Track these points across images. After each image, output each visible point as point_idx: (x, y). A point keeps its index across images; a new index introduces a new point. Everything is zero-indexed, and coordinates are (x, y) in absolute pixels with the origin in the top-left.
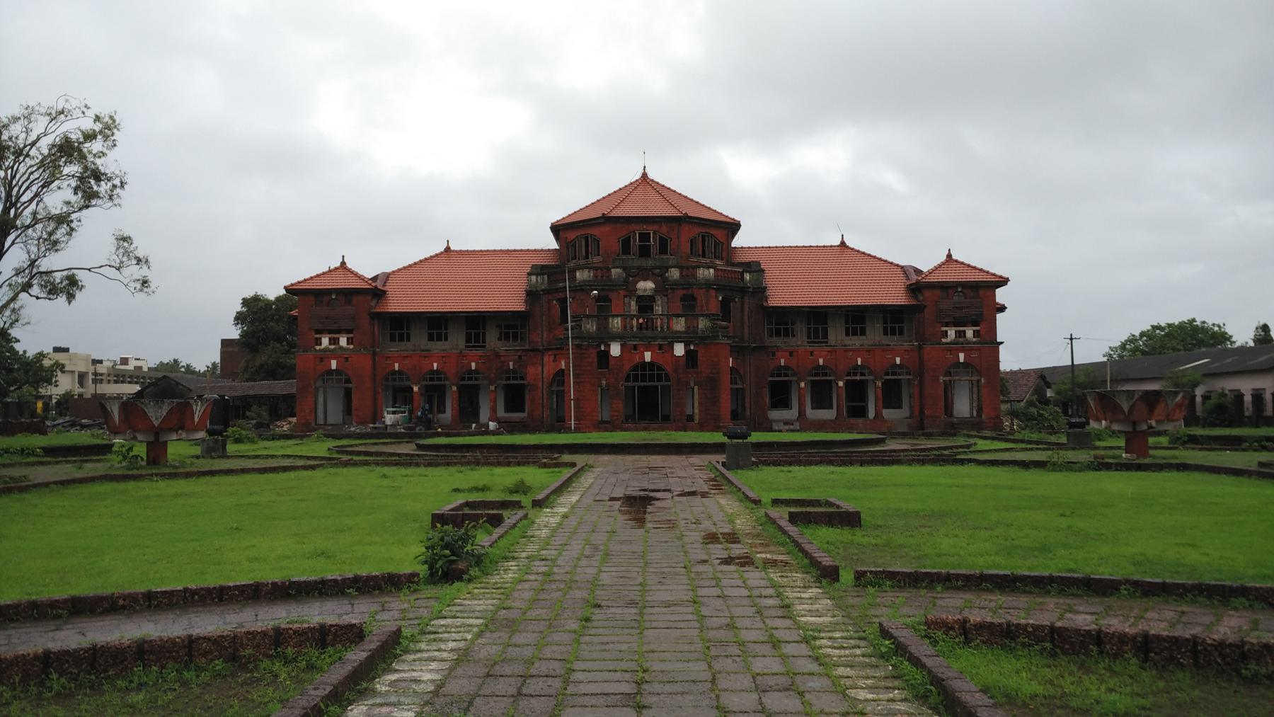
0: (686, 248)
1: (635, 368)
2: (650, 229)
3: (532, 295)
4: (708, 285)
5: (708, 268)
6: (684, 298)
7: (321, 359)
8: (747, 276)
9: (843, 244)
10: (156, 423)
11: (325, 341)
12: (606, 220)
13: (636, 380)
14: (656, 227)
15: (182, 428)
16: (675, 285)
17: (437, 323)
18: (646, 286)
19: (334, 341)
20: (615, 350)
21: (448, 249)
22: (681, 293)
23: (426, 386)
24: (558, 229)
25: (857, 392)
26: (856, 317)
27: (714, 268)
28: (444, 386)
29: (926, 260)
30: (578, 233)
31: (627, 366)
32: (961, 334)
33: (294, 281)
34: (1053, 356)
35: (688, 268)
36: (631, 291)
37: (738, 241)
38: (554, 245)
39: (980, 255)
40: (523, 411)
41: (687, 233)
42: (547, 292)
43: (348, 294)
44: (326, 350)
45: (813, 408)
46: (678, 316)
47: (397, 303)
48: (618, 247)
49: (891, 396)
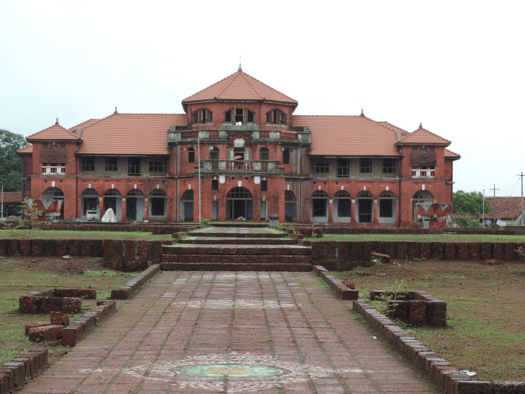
0: (264, 117)
1: (233, 190)
2: (243, 107)
3: (171, 145)
4: (275, 143)
5: (276, 132)
6: (262, 149)
7: (46, 181)
8: (300, 137)
9: (362, 115)
10: (47, 209)
11: (48, 170)
12: (217, 101)
13: (233, 197)
14: (247, 106)
15: (55, 211)
16: (256, 143)
17: (112, 162)
18: (239, 142)
19: (53, 170)
20: (222, 180)
21: (116, 113)
22: (259, 147)
23: (153, 199)
24: (186, 104)
25: (365, 206)
26: (366, 163)
27: (280, 132)
28: (115, 198)
29: (411, 127)
30: (199, 107)
31: (228, 189)
32: (423, 174)
33: (31, 134)
34: (468, 189)
35: (264, 132)
36: (230, 144)
37: (297, 112)
38: (182, 112)
39: (439, 129)
40: (162, 214)
41: (265, 110)
42: (181, 143)
43: (63, 143)
44: (48, 176)
45: (339, 216)
46: (257, 162)
47: (93, 147)
48: (223, 117)
49: (386, 209)
